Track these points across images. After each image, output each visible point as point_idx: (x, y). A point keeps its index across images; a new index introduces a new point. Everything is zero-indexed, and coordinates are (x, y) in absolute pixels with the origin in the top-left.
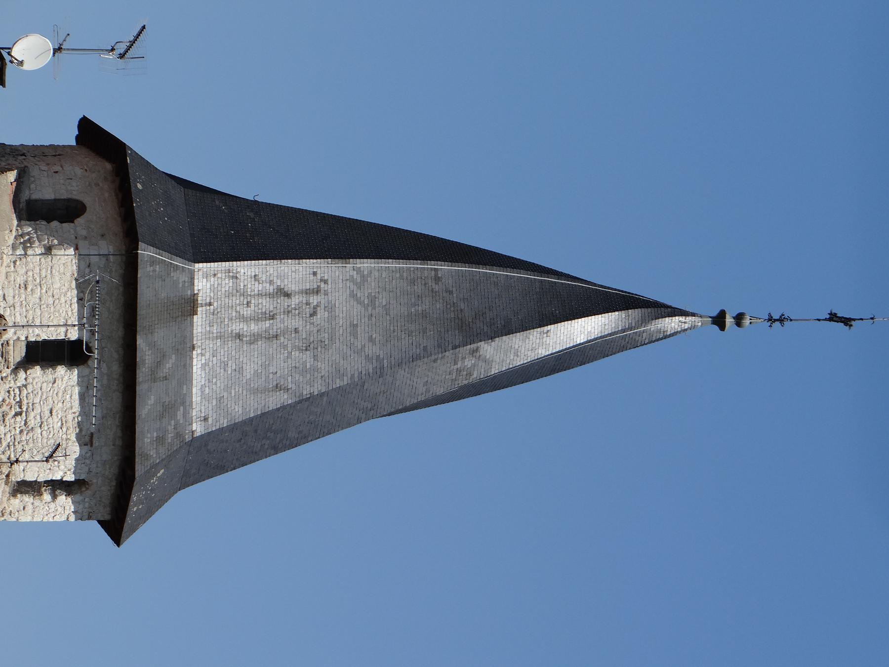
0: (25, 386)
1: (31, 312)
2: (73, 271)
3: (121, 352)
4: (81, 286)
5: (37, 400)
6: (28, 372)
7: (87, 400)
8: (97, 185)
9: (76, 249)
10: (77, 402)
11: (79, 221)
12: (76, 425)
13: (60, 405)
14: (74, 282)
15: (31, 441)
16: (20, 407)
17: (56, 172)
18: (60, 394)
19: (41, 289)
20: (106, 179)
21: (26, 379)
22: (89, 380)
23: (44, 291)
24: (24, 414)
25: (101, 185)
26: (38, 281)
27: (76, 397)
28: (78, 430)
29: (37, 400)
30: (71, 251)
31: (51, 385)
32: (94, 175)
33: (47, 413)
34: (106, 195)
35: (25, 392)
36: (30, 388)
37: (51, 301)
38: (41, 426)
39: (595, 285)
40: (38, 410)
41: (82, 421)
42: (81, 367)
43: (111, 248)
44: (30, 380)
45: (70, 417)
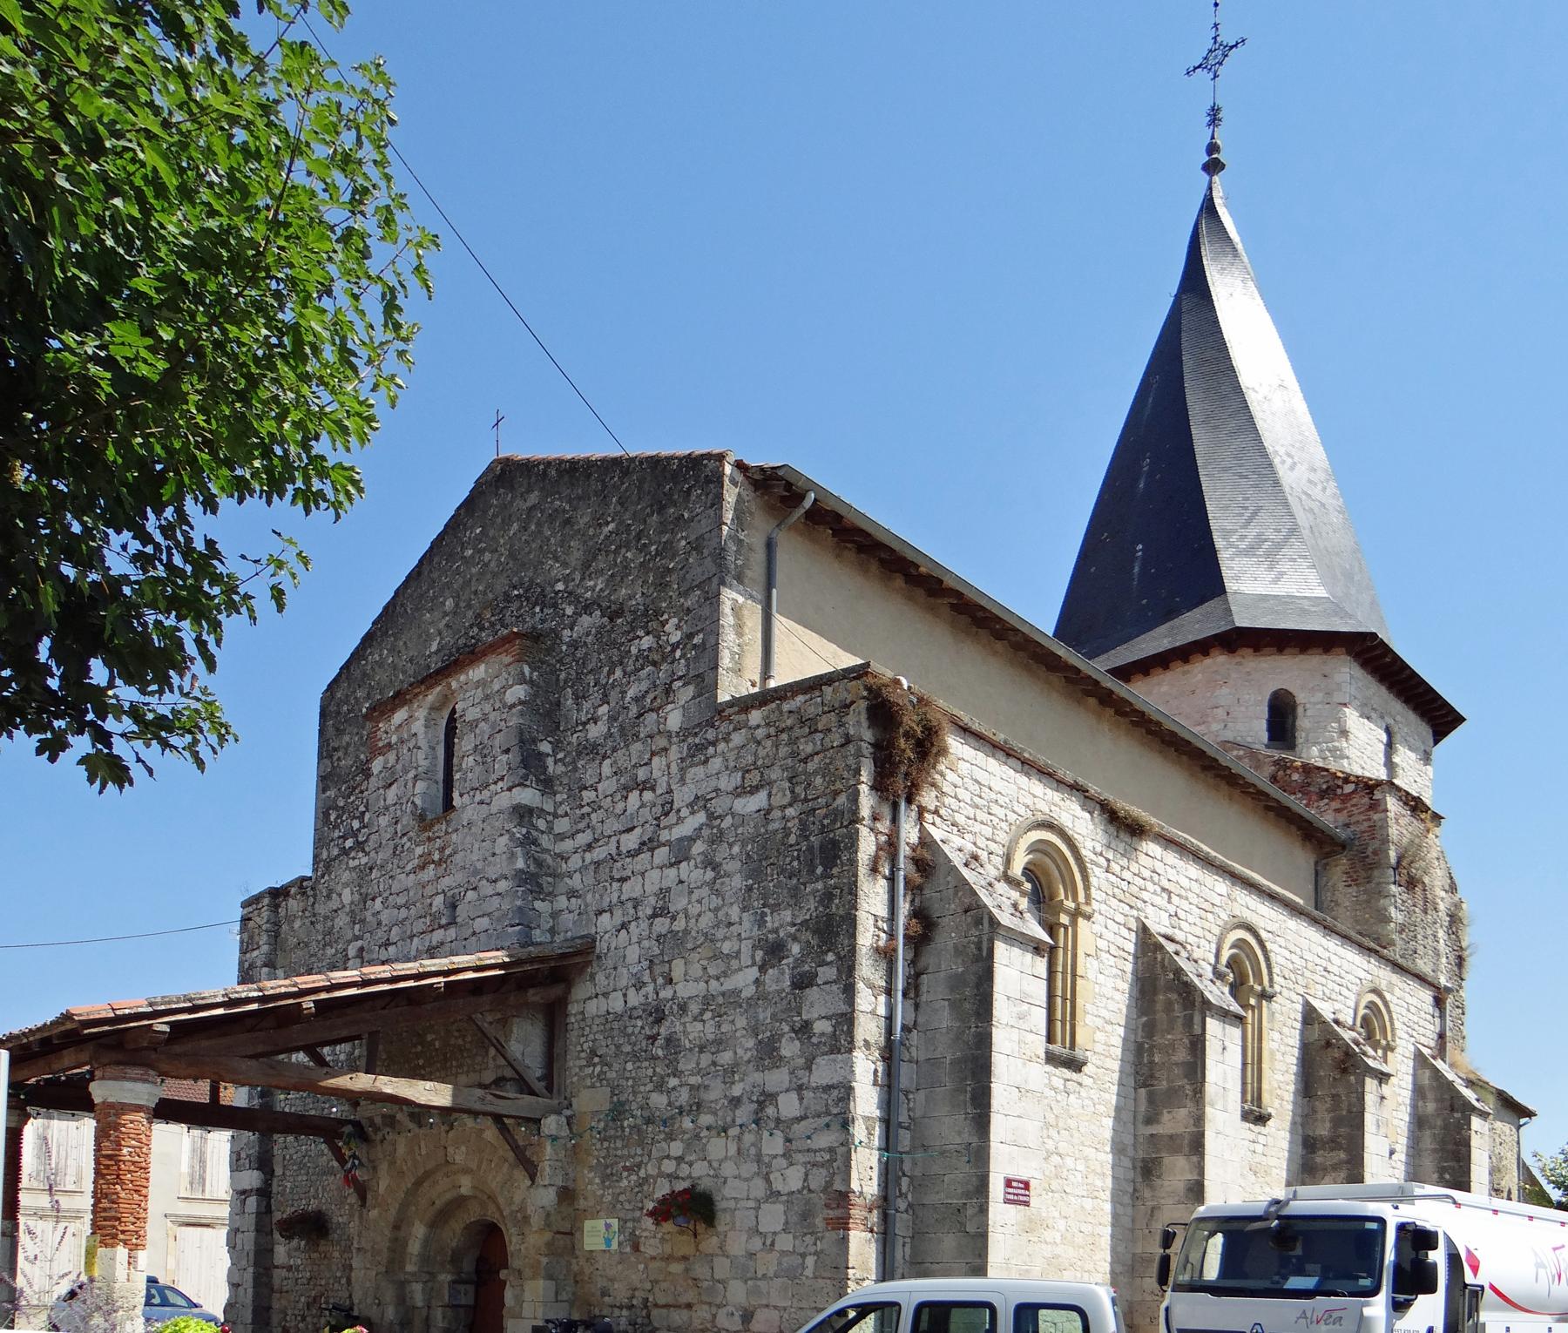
11: (1301, 697)
32: (1234, 675)
34: (1265, 665)
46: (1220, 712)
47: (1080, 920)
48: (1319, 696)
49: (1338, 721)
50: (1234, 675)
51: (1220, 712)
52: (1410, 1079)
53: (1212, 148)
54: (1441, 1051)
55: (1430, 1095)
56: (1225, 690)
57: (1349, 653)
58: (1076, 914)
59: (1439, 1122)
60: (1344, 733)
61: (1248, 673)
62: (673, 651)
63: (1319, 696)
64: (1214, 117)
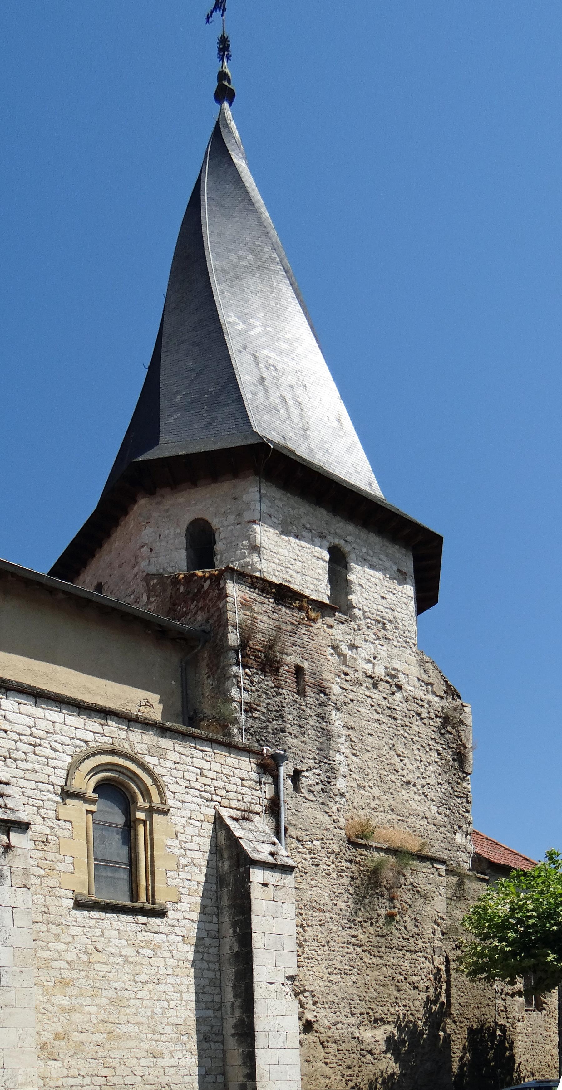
0: (364, 612)
1: (308, 585)
2: (274, 533)
3: (338, 518)
4: (285, 532)
5: (375, 606)
6: (355, 605)
7: (375, 564)
8: (167, 510)
9: (254, 522)
10: (376, 573)
11: (215, 523)
12: (392, 581)
13: (378, 588)
14: (283, 537)
15: (403, 622)
16: (379, 622)
17: (151, 550)
18: (371, 585)
19: (289, 568)
20: (159, 503)
21: (360, 610)
22: (360, 557)
23: (291, 567)
24: (385, 621)
25: (167, 507)
26: (283, 569)
27: (372, 572)
28: (395, 581)
29: (375, 606)
30: (257, 527)
31: (364, 590)
32: (155, 514)
33: (384, 601)
34: (181, 500)
35: (370, 615)
36: (366, 609)
37: (299, 564)
38: (393, 610)
39: (207, 151)
40: (381, 608)
41: (390, 575)
42: (348, 559)
43: (252, 489)
44: (360, 606)
45: (386, 583)
46: (145, 550)
47: (155, 816)
48: (231, 518)
49: (248, 538)
50: (155, 514)
51: (145, 550)
52: (208, 842)
53: (222, 76)
54: (66, 785)
55: (226, 854)
56: (149, 530)
57: (257, 473)
58: (151, 811)
59: (231, 879)
60: (255, 549)
61: (167, 510)
62: (264, 737)
63: (231, 518)
64: (224, 47)
